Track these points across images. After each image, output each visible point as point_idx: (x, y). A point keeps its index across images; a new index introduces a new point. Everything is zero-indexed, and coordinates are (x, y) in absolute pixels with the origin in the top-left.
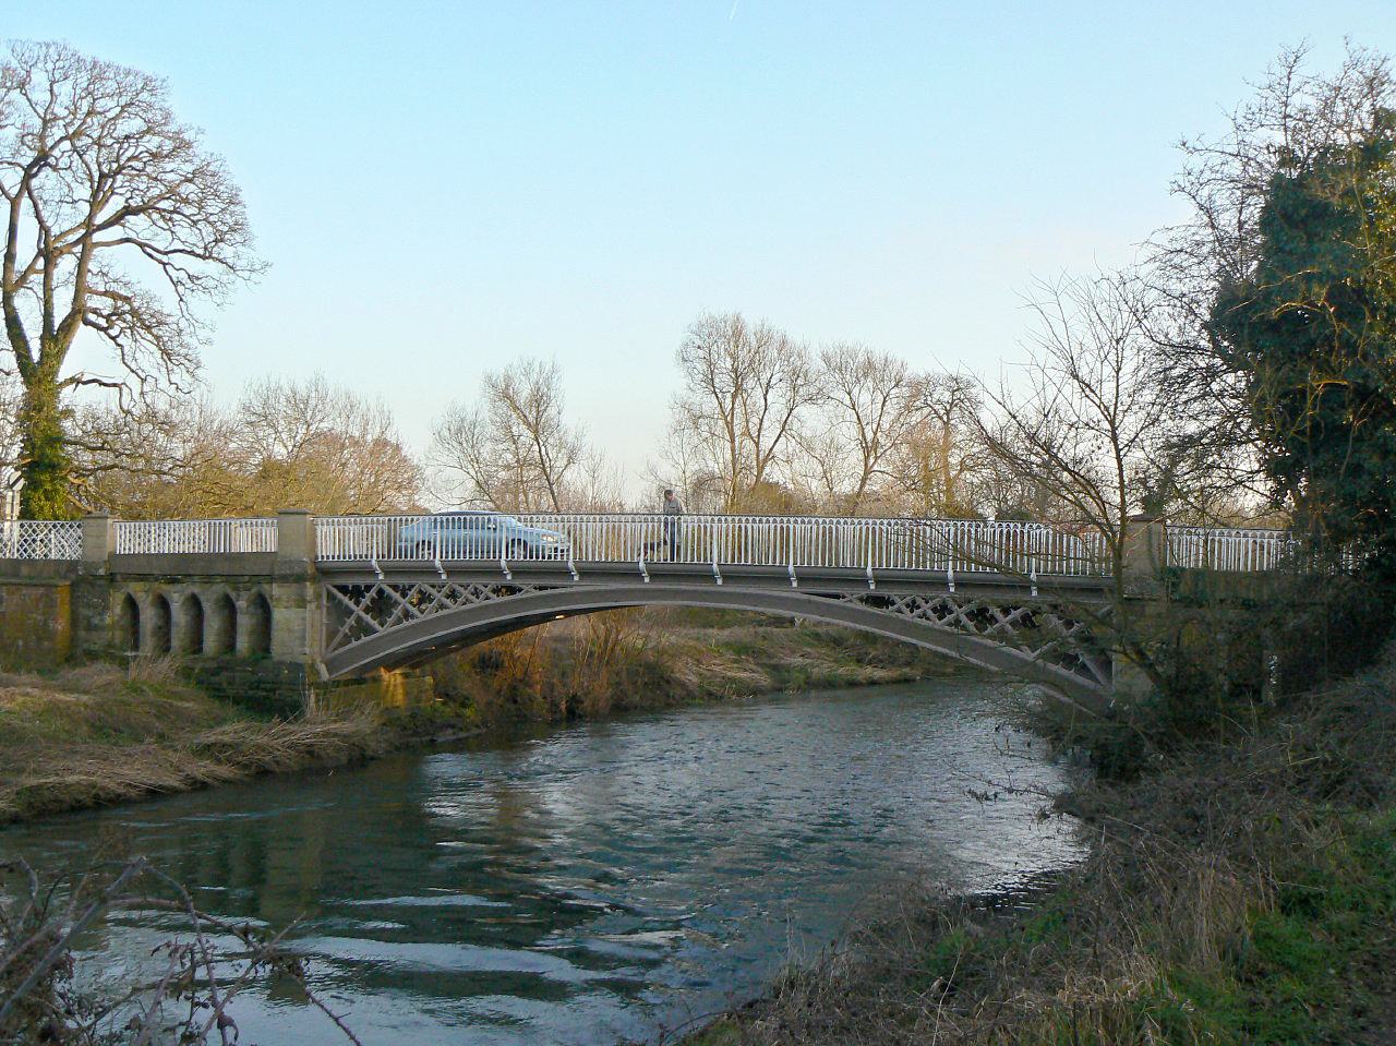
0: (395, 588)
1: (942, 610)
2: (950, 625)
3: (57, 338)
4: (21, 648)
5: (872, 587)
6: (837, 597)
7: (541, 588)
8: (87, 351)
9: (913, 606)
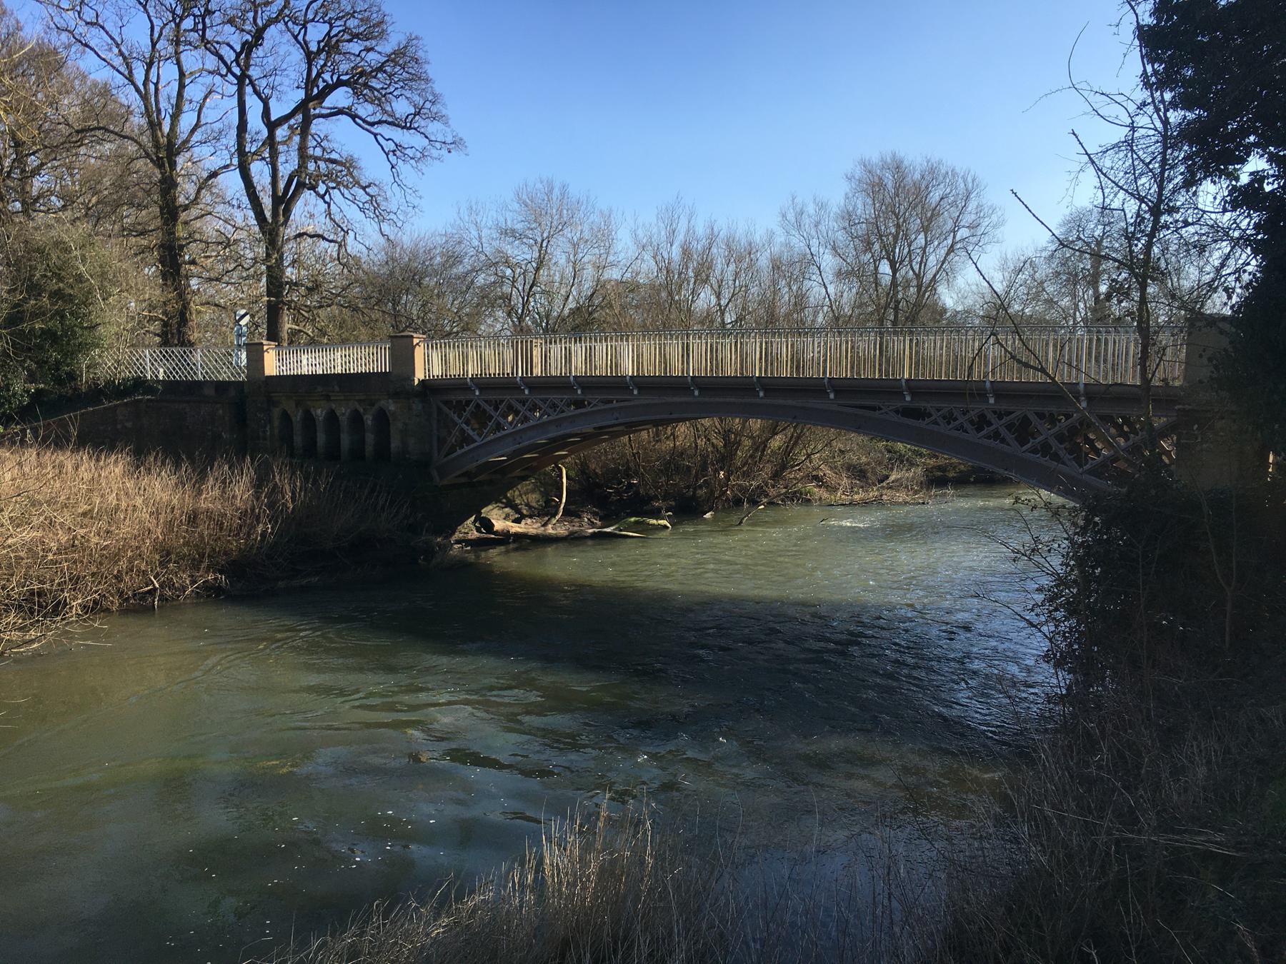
0: (1041, 416)
1: (981, 423)
2: (989, 437)
3: (284, 202)
4: (929, 789)
5: (908, 398)
6: (873, 409)
7: (873, 409)
8: (307, 212)
9: (949, 418)
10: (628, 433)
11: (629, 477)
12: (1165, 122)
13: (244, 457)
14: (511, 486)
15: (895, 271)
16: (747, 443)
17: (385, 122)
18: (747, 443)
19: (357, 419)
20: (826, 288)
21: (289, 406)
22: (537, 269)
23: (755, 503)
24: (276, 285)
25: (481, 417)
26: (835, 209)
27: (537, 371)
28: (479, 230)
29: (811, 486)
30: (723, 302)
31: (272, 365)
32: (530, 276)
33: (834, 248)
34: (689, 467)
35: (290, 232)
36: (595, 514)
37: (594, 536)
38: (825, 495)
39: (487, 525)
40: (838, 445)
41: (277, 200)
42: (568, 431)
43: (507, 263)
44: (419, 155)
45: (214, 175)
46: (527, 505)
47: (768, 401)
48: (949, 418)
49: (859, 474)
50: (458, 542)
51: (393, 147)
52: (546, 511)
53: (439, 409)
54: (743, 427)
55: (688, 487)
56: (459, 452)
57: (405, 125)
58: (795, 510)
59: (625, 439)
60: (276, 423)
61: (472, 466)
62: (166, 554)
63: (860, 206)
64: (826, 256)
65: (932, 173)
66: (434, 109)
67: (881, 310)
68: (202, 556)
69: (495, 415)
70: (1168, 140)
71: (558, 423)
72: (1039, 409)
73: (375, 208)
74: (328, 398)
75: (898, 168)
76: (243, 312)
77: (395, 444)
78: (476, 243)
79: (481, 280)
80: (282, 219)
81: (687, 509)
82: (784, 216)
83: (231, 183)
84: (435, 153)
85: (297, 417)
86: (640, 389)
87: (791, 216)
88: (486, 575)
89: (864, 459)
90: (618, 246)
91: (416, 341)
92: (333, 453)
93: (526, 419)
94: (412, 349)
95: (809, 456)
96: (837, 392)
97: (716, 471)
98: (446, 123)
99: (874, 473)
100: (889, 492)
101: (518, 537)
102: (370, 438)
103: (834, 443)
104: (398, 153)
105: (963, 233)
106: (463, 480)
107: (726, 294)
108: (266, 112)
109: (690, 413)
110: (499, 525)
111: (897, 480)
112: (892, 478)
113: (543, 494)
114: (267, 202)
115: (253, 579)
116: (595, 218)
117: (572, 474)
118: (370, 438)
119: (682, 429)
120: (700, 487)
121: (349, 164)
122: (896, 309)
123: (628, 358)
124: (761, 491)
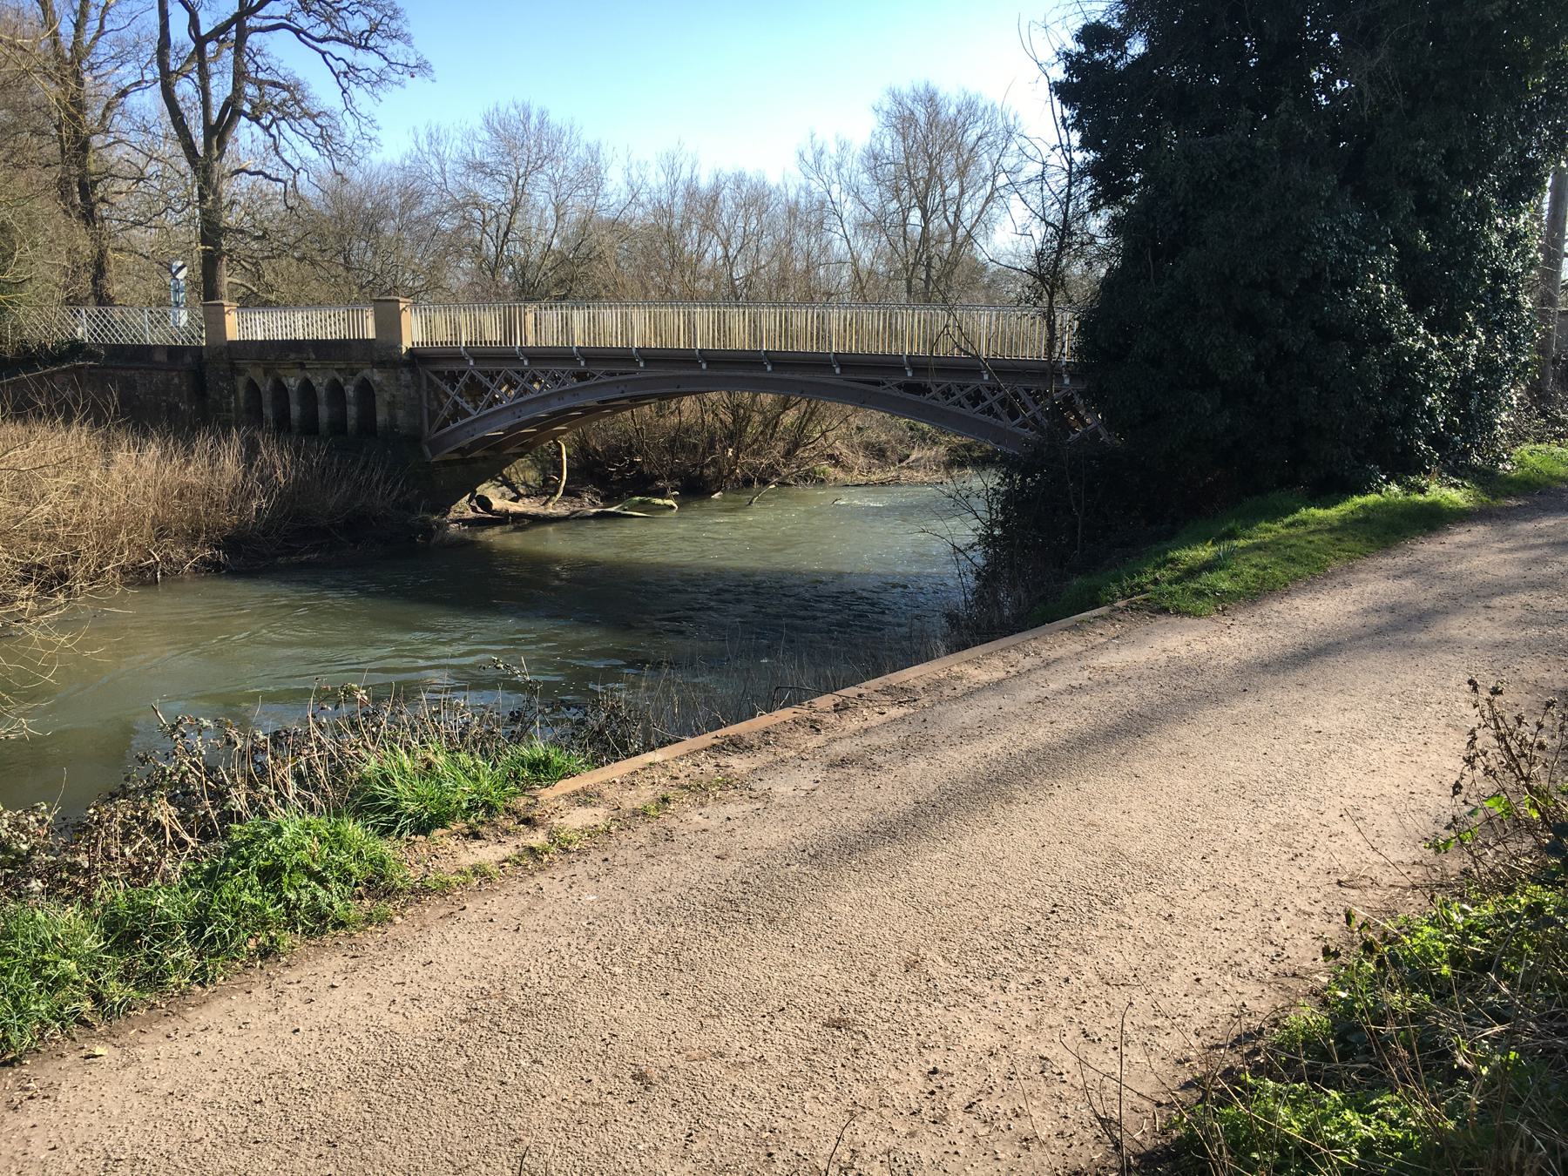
2: (983, 412)
3: (218, 132)
6: (877, 384)
7: (877, 384)
9: (948, 393)
10: (631, 407)
11: (630, 454)
12: (1070, 162)
13: (229, 432)
14: (508, 463)
15: (925, 218)
16: (757, 418)
17: (331, 39)
18: (757, 418)
19: (336, 390)
20: (848, 244)
21: (256, 374)
22: (513, 212)
23: (765, 483)
24: (211, 231)
25: (476, 390)
26: (859, 152)
27: (531, 342)
28: (442, 163)
29: (825, 465)
30: (732, 252)
31: (235, 327)
32: (504, 220)
33: (857, 193)
34: (695, 446)
35: (228, 163)
36: (596, 494)
37: (597, 516)
38: (841, 475)
39: (485, 503)
40: (855, 421)
41: (210, 130)
42: (571, 404)
43: (477, 205)
44: (374, 78)
45: (124, 93)
46: (524, 483)
47: (775, 375)
48: (948, 393)
49: (878, 453)
50: (456, 521)
51: (343, 67)
52: (545, 490)
53: (430, 383)
54: (753, 400)
55: (695, 466)
56: (453, 426)
57: (359, 42)
58: (809, 490)
59: (628, 414)
60: (242, 393)
61: (465, 442)
62: (161, 531)
63: (888, 144)
64: (848, 205)
65: (970, 109)
66: (394, 25)
67: (910, 270)
68: (198, 532)
69: (492, 386)
70: (1074, 176)
71: (560, 395)
72: (1028, 385)
73: (325, 140)
74: (302, 366)
75: (931, 100)
76: (180, 263)
77: (381, 417)
78: (438, 179)
79: (447, 225)
80: (216, 153)
81: (694, 489)
82: (801, 155)
83: (148, 102)
84: (395, 77)
85: (266, 387)
86: (646, 361)
87: (809, 157)
88: (486, 554)
89: (883, 437)
90: (609, 187)
91: (402, 306)
92: (310, 427)
93: (526, 391)
94: (398, 315)
95: (823, 433)
96: (842, 367)
97: (725, 449)
98: (408, 42)
99: (894, 450)
100: (907, 472)
101: (518, 517)
102: (352, 411)
103: (851, 419)
104: (351, 75)
105: (1002, 180)
106: (456, 456)
107: (735, 245)
108: (194, 23)
109: (698, 387)
110: (497, 504)
111: (917, 460)
112: (912, 458)
113: (543, 471)
114: (198, 134)
115: (247, 553)
116: (580, 152)
117: (571, 451)
118: (352, 411)
119: (688, 403)
120: (708, 466)
121: (293, 89)
122: (929, 266)
123: (633, 326)
124: (772, 470)
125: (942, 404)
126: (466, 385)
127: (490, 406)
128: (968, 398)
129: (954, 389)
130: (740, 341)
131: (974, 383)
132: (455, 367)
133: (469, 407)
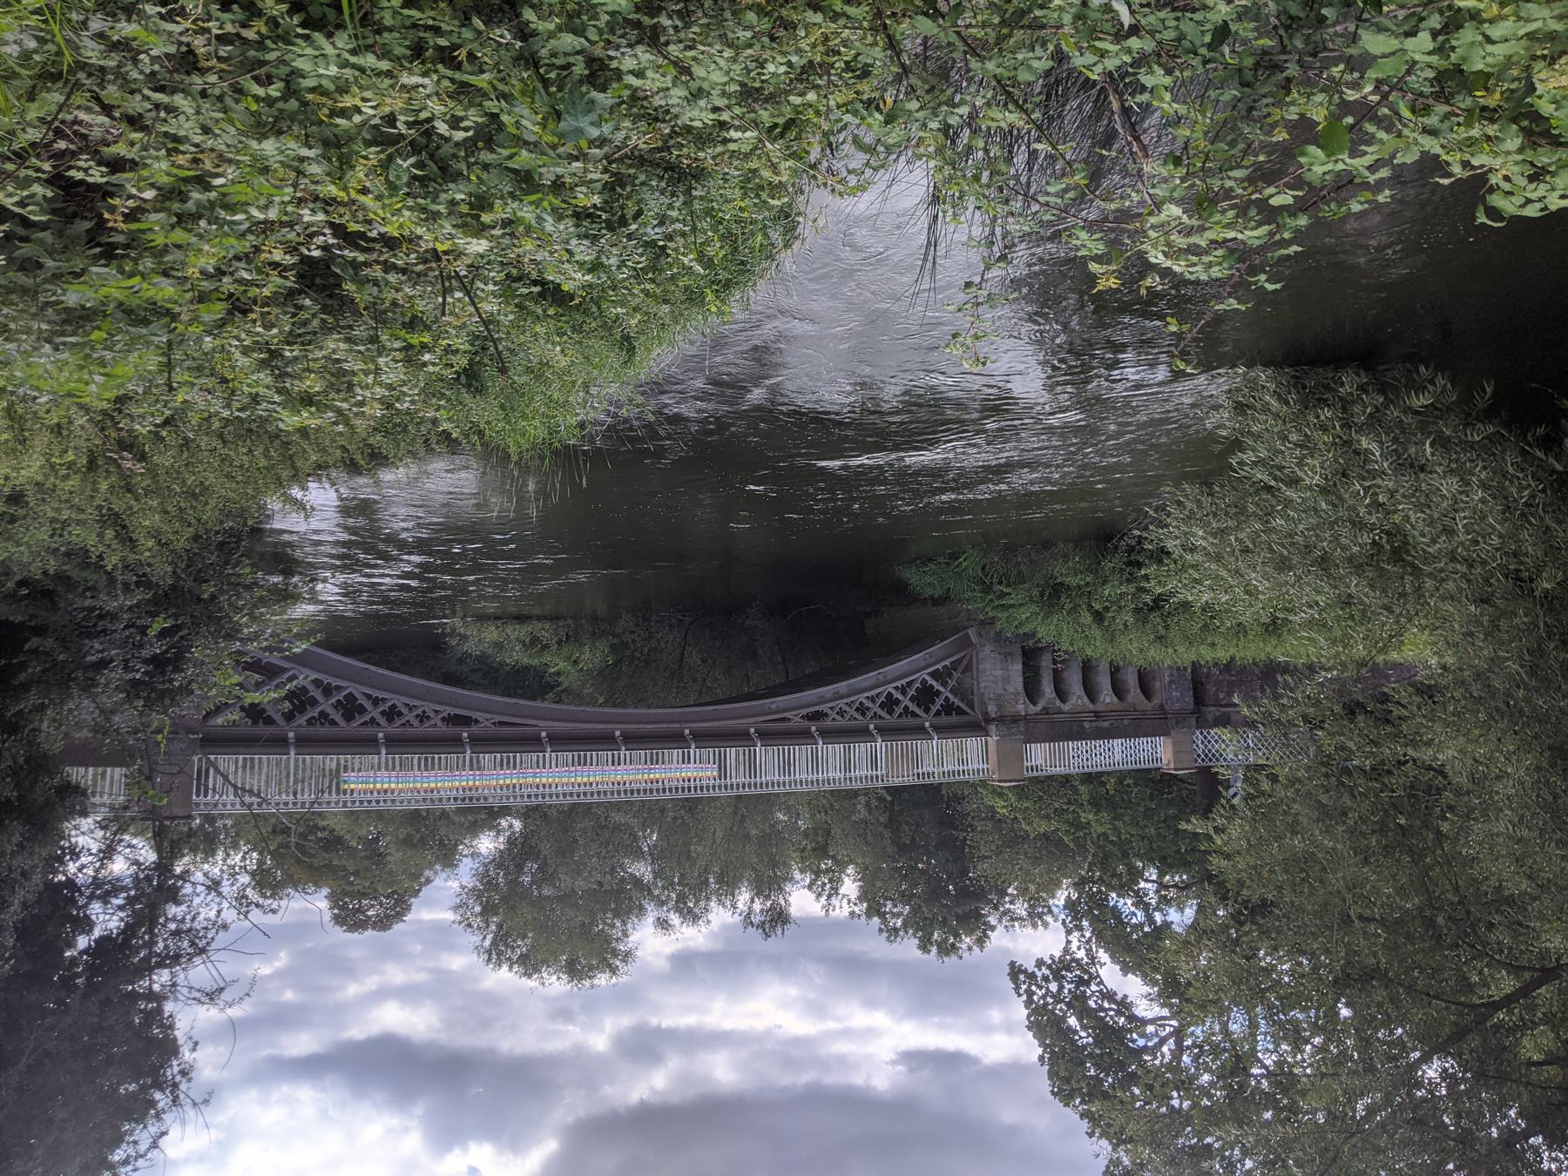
6: (501, 723)
56: (947, 662)
125: (429, 707)
126: (933, 702)
127: (910, 684)
128: (400, 714)
129: (416, 723)
130: (765, 754)
131: (395, 728)
132: (944, 719)
133: (928, 678)
